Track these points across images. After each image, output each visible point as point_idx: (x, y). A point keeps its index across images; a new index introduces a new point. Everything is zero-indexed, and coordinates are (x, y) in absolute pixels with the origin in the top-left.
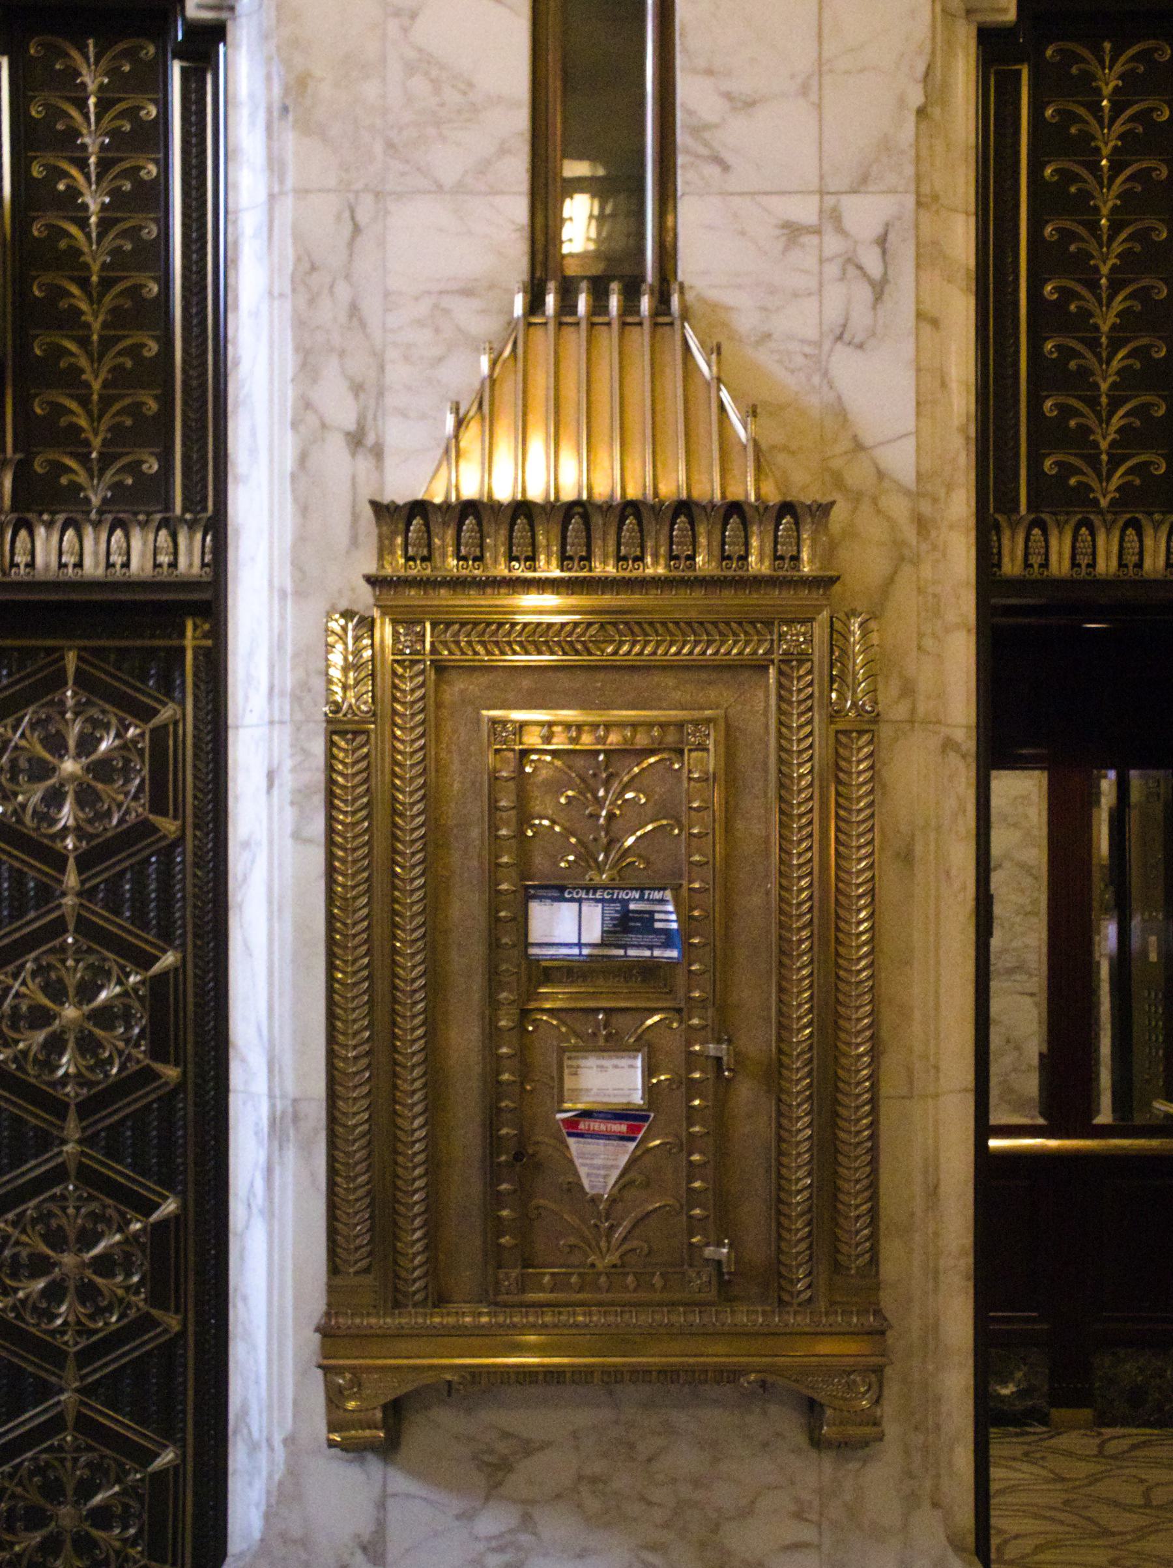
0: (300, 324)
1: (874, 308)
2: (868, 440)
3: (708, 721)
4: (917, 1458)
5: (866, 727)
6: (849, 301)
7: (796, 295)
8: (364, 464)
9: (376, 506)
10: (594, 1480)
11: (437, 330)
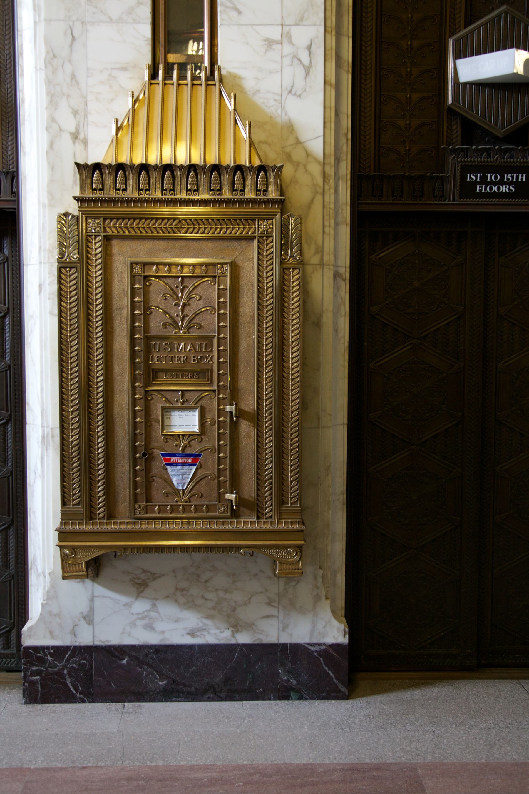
0: (49, 82)
1: (306, 78)
2: (302, 139)
3: (226, 264)
4: (320, 580)
5: (296, 266)
6: (294, 76)
7: (271, 72)
8: (79, 147)
9: (77, 164)
10: (182, 590)
11: (111, 87)
